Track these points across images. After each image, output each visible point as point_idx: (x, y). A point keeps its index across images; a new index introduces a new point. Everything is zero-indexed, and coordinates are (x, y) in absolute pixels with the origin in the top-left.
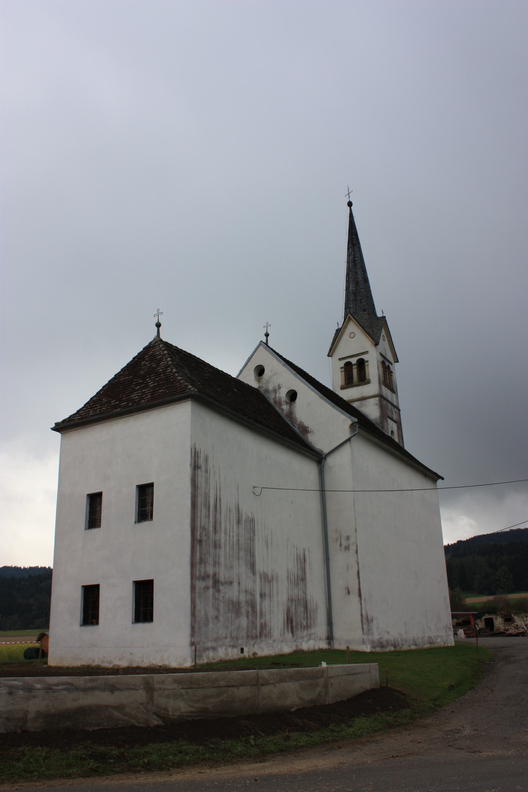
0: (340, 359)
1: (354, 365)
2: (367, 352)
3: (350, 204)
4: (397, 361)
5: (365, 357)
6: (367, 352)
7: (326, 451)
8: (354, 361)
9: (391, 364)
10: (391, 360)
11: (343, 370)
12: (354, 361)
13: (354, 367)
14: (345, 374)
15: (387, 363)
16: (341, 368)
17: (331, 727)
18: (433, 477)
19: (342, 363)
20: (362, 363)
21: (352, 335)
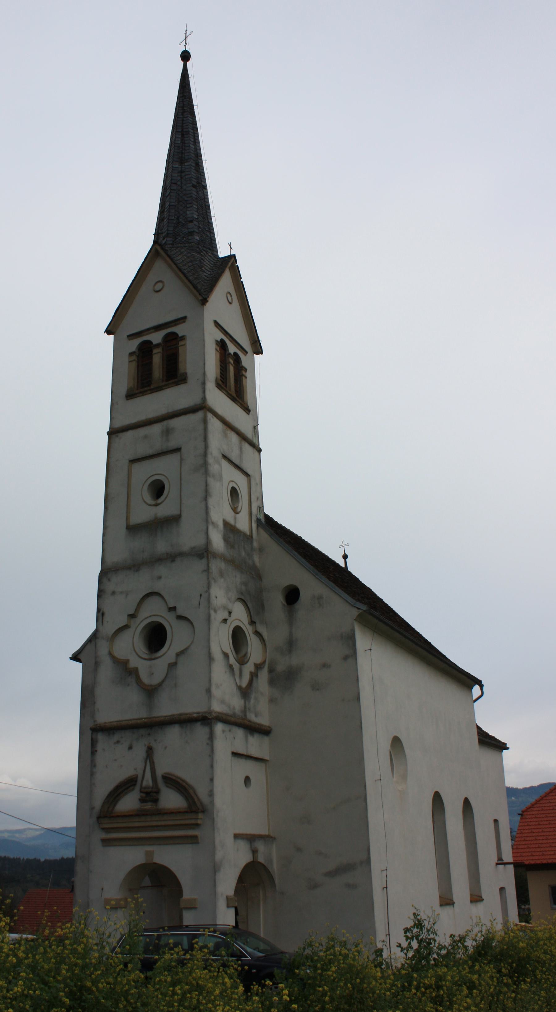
0: (131, 337)
1: (158, 345)
2: (185, 318)
3: (186, 56)
4: (258, 350)
5: (179, 330)
6: (183, 319)
7: (178, 513)
8: (157, 338)
9: (245, 352)
10: (245, 342)
11: (134, 357)
12: (157, 338)
13: (155, 351)
14: (138, 366)
15: (232, 349)
16: (131, 354)
17: (47, 967)
18: (224, 457)
19: (134, 344)
20: (173, 343)
21: (159, 286)
